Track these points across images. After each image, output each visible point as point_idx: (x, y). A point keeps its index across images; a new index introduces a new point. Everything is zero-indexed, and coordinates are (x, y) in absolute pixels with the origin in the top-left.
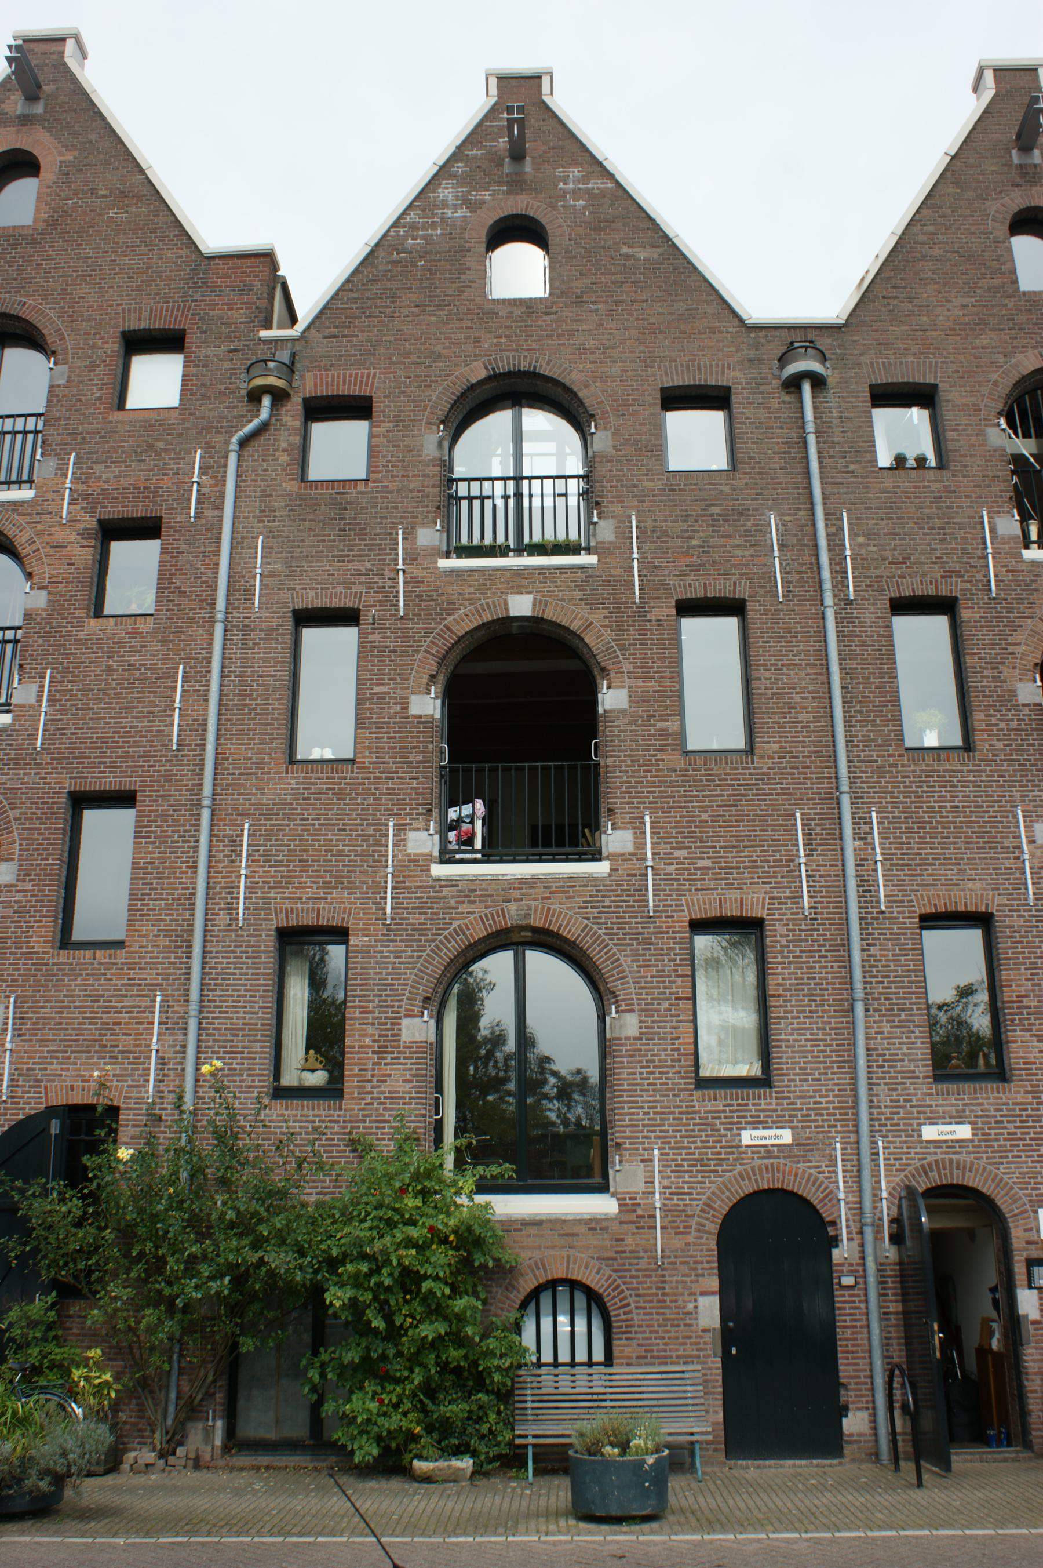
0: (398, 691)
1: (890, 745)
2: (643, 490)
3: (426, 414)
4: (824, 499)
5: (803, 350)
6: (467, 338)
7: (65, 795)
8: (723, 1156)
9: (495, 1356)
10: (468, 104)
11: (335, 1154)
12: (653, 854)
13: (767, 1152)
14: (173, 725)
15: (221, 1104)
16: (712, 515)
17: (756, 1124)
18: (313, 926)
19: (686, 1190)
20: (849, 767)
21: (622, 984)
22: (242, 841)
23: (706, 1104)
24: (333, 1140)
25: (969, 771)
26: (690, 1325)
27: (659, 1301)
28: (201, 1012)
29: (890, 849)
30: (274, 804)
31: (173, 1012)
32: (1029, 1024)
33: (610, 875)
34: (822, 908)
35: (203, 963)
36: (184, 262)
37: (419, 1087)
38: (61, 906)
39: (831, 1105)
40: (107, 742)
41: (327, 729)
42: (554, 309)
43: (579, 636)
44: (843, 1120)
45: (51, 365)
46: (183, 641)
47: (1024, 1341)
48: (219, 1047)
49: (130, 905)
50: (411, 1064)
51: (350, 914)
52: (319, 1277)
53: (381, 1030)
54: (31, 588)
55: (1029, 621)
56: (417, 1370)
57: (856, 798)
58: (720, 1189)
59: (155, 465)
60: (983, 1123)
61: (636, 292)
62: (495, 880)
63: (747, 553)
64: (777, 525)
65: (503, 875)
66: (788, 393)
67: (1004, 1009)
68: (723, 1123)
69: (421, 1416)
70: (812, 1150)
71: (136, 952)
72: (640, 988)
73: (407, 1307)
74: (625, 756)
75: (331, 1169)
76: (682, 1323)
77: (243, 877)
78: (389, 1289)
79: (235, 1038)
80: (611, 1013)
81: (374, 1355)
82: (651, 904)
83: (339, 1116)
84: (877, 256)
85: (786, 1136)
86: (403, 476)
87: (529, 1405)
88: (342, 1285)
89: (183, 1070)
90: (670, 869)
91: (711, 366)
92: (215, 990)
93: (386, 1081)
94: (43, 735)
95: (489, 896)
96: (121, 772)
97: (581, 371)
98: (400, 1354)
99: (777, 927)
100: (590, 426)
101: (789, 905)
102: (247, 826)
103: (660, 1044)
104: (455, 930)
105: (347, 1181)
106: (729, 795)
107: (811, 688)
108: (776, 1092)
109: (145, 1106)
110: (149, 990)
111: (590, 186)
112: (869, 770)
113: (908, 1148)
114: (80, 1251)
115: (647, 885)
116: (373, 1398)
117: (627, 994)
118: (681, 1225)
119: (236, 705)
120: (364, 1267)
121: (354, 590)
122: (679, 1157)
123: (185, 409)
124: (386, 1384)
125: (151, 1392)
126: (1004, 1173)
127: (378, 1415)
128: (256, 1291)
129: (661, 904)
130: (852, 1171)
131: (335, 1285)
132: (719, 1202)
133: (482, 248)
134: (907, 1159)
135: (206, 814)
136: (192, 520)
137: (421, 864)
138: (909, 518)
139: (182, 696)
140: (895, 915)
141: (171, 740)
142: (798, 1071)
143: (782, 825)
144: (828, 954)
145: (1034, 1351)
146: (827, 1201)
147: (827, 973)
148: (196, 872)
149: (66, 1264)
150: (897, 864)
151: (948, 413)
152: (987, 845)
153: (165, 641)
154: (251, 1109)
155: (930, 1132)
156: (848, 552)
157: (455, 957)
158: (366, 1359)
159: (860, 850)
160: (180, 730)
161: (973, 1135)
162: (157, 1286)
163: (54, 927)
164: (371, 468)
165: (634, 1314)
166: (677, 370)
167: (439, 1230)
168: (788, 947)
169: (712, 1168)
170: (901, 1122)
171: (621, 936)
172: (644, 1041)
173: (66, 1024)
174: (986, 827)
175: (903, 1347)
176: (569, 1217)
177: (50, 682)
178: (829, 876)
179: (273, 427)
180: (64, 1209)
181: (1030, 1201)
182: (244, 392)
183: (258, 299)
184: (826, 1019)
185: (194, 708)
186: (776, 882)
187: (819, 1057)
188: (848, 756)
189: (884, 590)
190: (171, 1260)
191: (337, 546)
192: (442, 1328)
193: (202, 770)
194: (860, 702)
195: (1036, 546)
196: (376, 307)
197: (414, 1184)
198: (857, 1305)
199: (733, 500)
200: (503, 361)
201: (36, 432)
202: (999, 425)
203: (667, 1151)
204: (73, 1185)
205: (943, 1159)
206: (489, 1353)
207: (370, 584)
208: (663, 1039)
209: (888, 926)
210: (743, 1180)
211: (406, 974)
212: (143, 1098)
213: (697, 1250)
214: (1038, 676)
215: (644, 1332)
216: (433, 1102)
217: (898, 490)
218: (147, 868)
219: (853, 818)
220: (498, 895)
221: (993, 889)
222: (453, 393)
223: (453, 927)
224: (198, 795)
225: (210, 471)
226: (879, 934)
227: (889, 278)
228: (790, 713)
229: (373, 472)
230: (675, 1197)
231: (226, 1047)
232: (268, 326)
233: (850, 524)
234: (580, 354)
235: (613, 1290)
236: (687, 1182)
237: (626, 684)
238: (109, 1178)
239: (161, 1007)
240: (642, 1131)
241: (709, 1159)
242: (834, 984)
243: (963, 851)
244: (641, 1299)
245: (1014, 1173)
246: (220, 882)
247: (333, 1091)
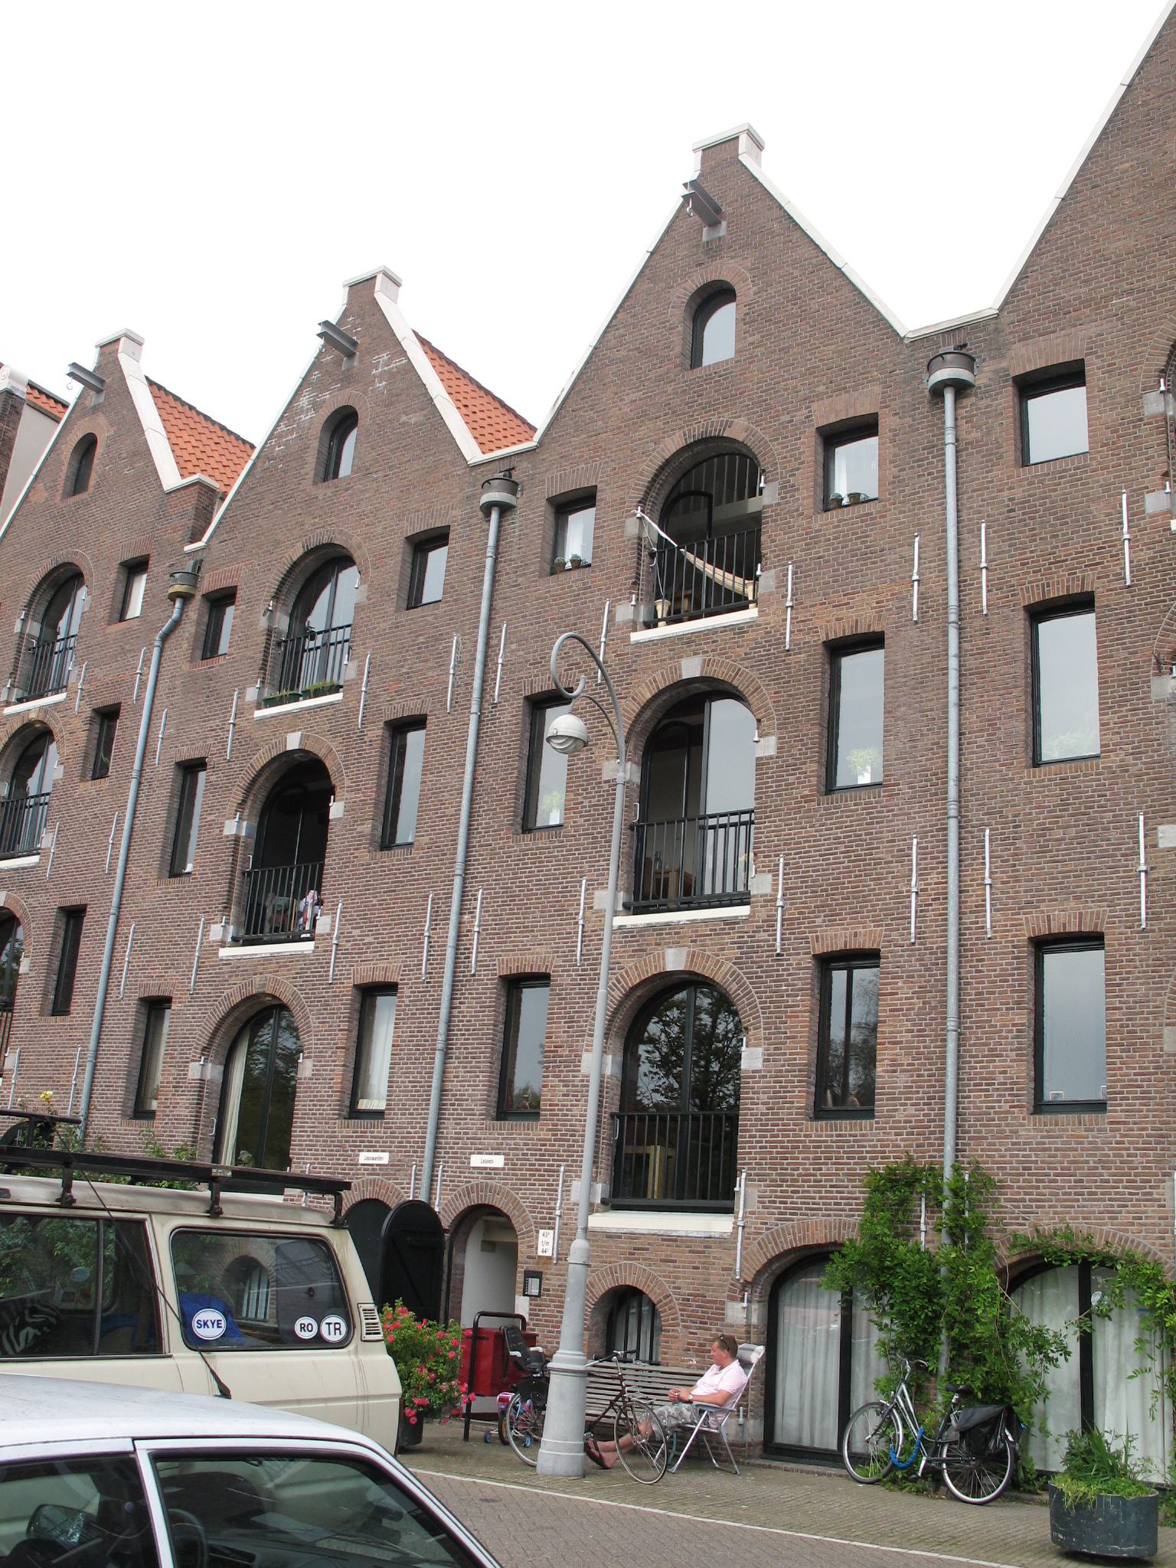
17: (371, 1148)
62: (251, 959)
85: (384, 1158)
155: (476, 1160)
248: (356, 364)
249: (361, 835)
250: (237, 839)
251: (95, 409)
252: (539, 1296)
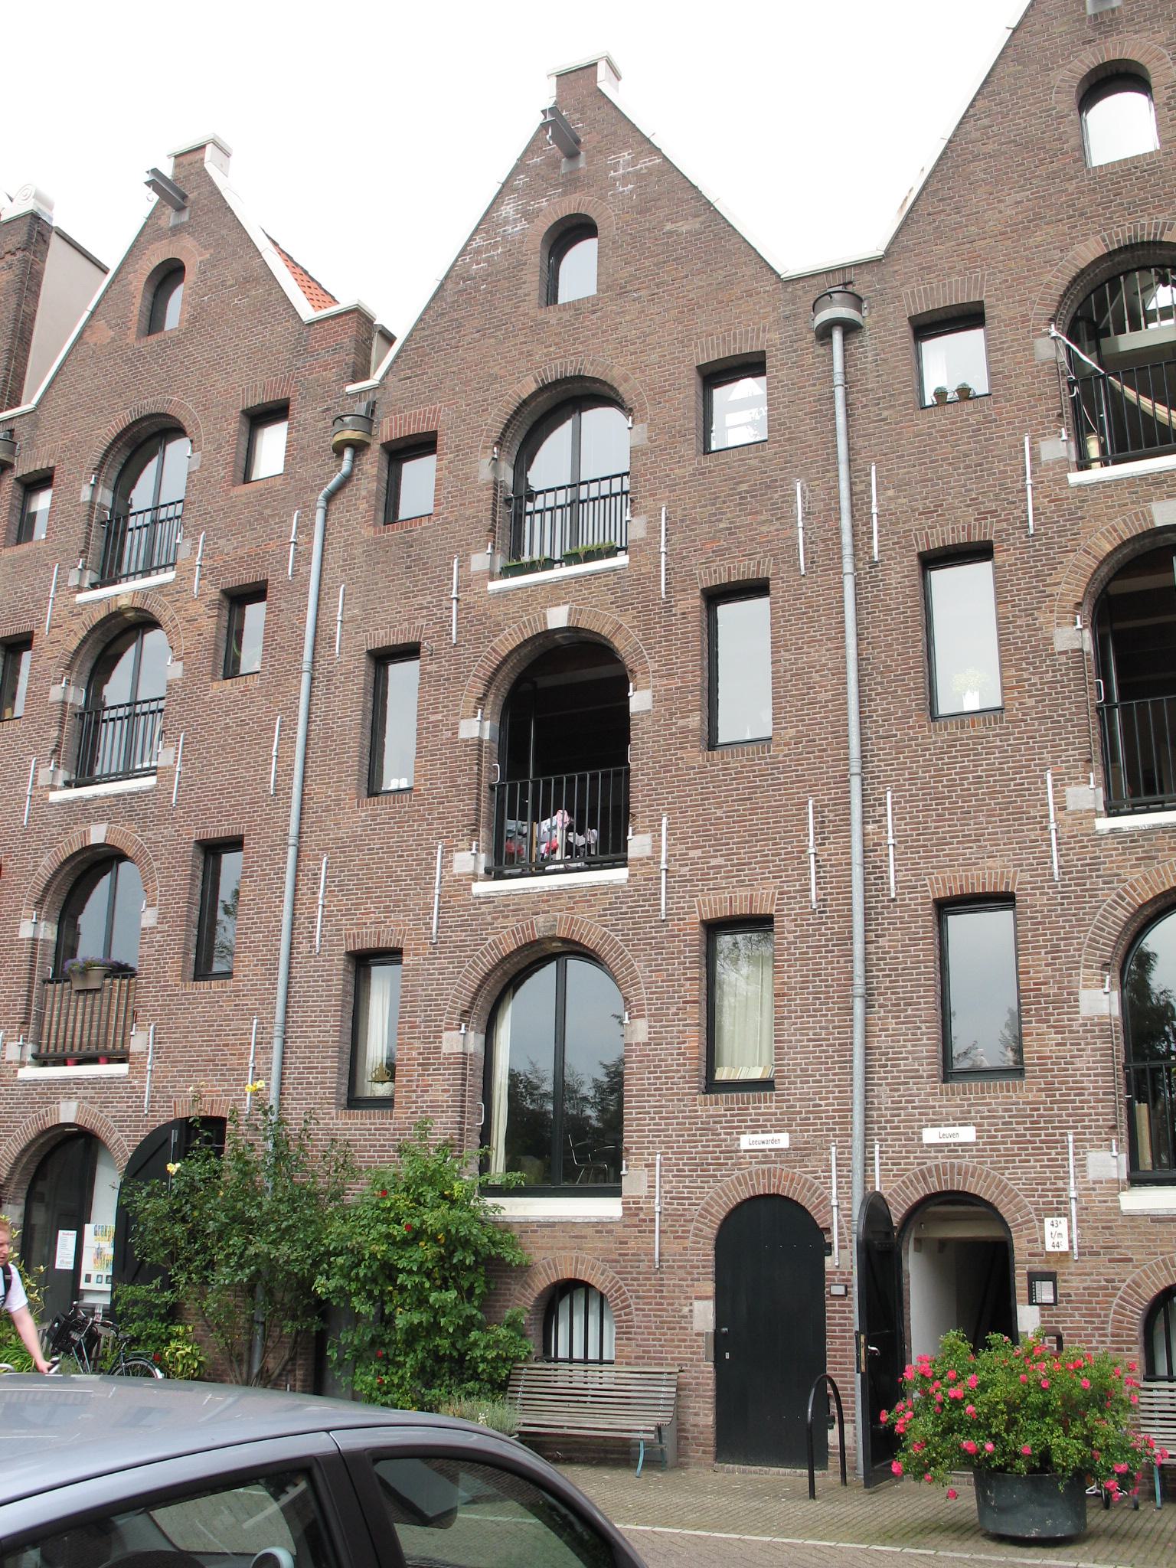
13: (764, 1156)
16: (740, 493)
17: (756, 1128)
26: (685, 1328)
28: (285, 1033)
62: (526, 893)
63: (773, 528)
85: (783, 1140)
90: (685, 870)
155: (930, 1135)
248: (581, 165)
249: (685, 731)
250: (480, 741)
251: (176, 230)
252: (1055, 1303)
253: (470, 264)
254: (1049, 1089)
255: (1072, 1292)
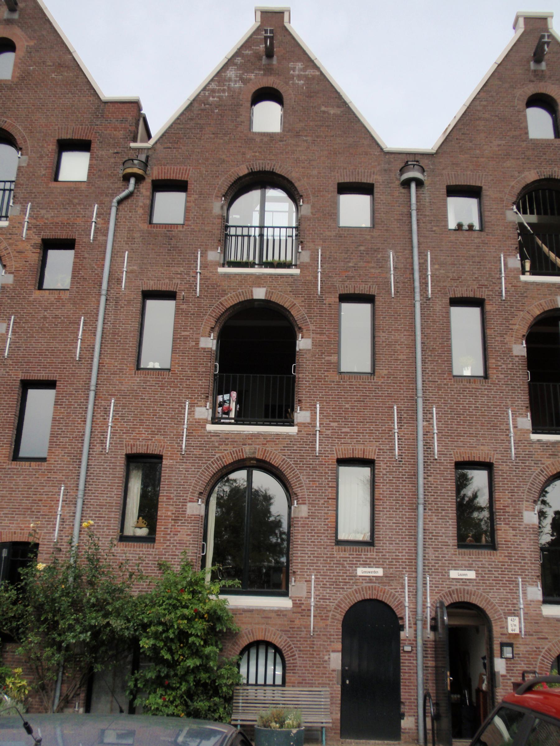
0: (194, 335)
1: (445, 374)
2: (325, 236)
3: (215, 191)
4: (418, 245)
5: (412, 166)
6: (239, 152)
7: (19, 382)
8: (347, 581)
9: (224, 678)
10: (246, 25)
11: (149, 571)
12: (320, 424)
13: (370, 579)
14: (77, 348)
15: (92, 543)
16: (360, 251)
17: (365, 565)
18: (145, 454)
19: (327, 597)
20: (423, 384)
21: (301, 490)
22: (110, 408)
23: (339, 554)
24: (149, 564)
25: (485, 389)
26: (325, 667)
27: (311, 654)
28: (84, 496)
29: (442, 427)
30: (128, 390)
31: (70, 495)
32: (509, 521)
33: (297, 434)
34: (405, 456)
35: (87, 470)
36: (91, 104)
37: (194, 538)
38: (14, 438)
39: (404, 557)
40: (42, 355)
41: (157, 351)
42: (285, 139)
43: (288, 311)
44: (410, 565)
45: (19, 156)
46: (84, 304)
47: (497, 685)
48: (93, 514)
49: (50, 439)
50: (191, 526)
51: (164, 448)
52: (137, 633)
53: (177, 508)
54: (5, 273)
55: (521, 313)
56: (184, 684)
57: (426, 400)
58: (345, 598)
59: (73, 212)
60: (482, 571)
61: (328, 131)
62: (239, 434)
63: (377, 271)
64: (393, 257)
65: (243, 431)
66: (404, 188)
67: (496, 512)
68: (348, 564)
69: (185, 708)
70: (392, 580)
71: (52, 464)
72: (310, 492)
73: (181, 651)
74: (309, 373)
75: (146, 579)
76: (321, 666)
77: (110, 427)
78: (172, 640)
79: (101, 510)
80: (294, 504)
81: (163, 675)
82: (317, 449)
83: (152, 551)
84: (455, 117)
85: (380, 572)
86: (202, 223)
87: (240, 705)
88: (148, 638)
89: (73, 525)
90: (328, 432)
91: (364, 172)
92: (92, 485)
93: (177, 534)
94: (9, 350)
95: (235, 442)
96: (49, 371)
97: (297, 172)
98: (176, 675)
99: (381, 464)
100: (300, 201)
101: (388, 454)
102: (113, 401)
103: (318, 521)
104: (217, 458)
105: (155, 585)
106: (360, 396)
107: (406, 343)
108: (376, 549)
109: (52, 544)
110: (58, 484)
111: (307, 73)
112: (433, 386)
113: (442, 581)
114: (14, 617)
115: (316, 440)
116: (160, 697)
117: (303, 495)
118: (324, 615)
119: (110, 338)
120: (160, 629)
121: (174, 282)
122: (325, 580)
123: (90, 183)
124: (168, 690)
125: (47, 692)
126: (491, 598)
127: (162, 706)
128: (104, 641)
129: (323, 449)
130: (413, 592)
131: (145, 637)
132: (344, 604)
133: (249, 104)
134: (442, 587)
135: (92, 394)
136: (91, 241)
137: (201, 424)
138: (463, 256)
139: (82, 333)
140: (442, 461)
141: (76, 355)
142: (388, 539)
143: (387, 412)
144: (407, 479)
145: (502, 691)
146: (399, 606)
147: (405, 489)
148: (85, 424)
149: (6, 624)
150: (445, 435)
151: (486, 201)
152: (492, 428)
153: (75, 304)
154: (107, 546)
155: (454, 574)
156: (429, 273)
157: (216, 472)
158: (158, 677)
159: (426, 427)
160: (81, 350)
161: (476, 577)
162: (53, 636)
163: (10, 449)
164: (186, 218)
165: (298, 660)
166: (346, 174)
167: (200, 612)
168: (386, 475)
169: (341, 586)
170: (440, 568)
171: (301, 465)
172: (310, 519)
173: (14, 500)
174: (492, 418)
175: (434, 685)
176: (267, 609)
177: (14, 322)
178: (409, 439)
179: (135, 195)
180: (7, 595)
181: (504, 613)
182: (121, 175)
183: (130, 126)
184: (404, 513)
185: (88, 339)
186: (382, 441)
187: (399, 532)
188: (423, 378)
189: (447, 293)
190: (61, 622)
191: (166, 259)
192: (198, 662)
193: (91, 371)
194: (431, 351)
195: (528, 273)
196: (192, 133)
197: (188, 587)
198: (412, 661)
199: (372, 243)
200: (256, 165)
201: (10, 190)
202: (512, 209)
203: (319, 577)
204: (12, 583)
205: (460, 588)
206: (221, 677)
207: (182, 279)
208: (320, 519)
209: (438, 467)
210: (357, 593)
211: (191, 480)
212: (52, 539)
213: (332, 629)
214: (524, 342)
215: (302, 670)
216: (201, 546)
217: (458, 242)
218: (60, 421)
219: (424, 410)
220: (240, 442)
221: (494, 451)
222: (230, 181)
223: (216, 457)
224: (89, 384)
225: (102, 216)
226: (434, 470)
227: (460, 129)
228: (394, 355)
229: (187, 220)
230: (322, 601)
231: (96, 514)
232: (135, 140)
233: (431, 258)
234: (297, 163)
235: (288, 647)
236: (328, 593)
237: (311, 336)
238: (31, 579)
239: (64, 492)
240: (307, 566)
241: (340, 582)
242: (409, 495)
243: (480, 430)
244: (301, 653)
245: (496, 598)
246: (97, 429)
247: (150, 538)
252: (513, 657)
253: (209, 97)
254: (509, 556)
255: (520, 653)
